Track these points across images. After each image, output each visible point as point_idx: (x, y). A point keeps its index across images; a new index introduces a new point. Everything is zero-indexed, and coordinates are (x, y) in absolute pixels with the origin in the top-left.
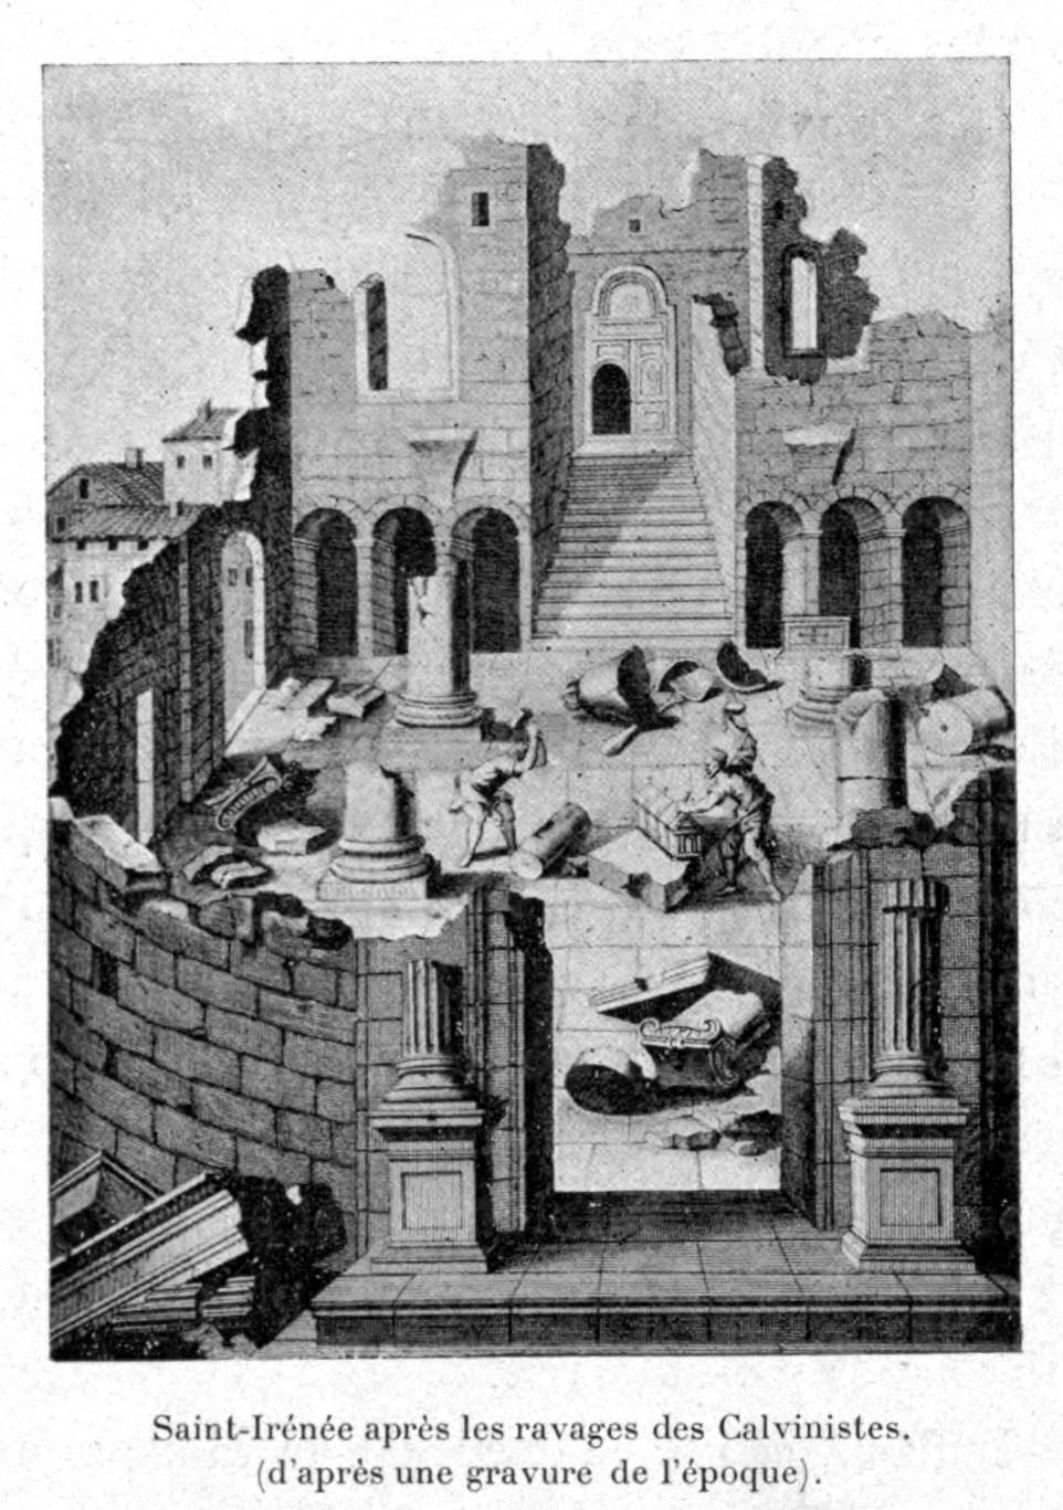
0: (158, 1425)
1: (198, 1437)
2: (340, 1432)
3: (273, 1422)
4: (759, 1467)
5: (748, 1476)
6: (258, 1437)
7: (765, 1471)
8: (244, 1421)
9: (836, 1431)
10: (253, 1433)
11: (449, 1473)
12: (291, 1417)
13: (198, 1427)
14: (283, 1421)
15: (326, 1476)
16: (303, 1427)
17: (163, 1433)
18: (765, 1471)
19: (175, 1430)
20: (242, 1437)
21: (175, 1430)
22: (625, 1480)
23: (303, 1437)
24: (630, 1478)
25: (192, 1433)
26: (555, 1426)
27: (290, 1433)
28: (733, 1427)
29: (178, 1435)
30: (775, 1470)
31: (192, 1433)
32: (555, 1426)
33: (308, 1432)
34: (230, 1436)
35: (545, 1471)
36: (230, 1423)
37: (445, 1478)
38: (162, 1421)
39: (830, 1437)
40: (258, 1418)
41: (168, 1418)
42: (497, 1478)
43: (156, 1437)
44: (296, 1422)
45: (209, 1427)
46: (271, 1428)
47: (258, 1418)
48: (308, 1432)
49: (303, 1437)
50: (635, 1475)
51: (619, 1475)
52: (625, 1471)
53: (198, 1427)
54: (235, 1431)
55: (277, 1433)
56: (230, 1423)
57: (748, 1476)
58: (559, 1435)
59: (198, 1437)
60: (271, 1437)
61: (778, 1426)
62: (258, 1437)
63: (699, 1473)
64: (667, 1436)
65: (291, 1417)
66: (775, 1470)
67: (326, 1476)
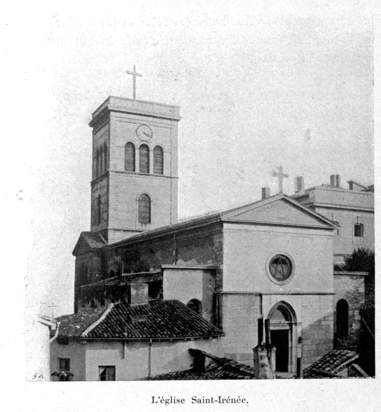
2: (242, 401)
6: (220, 402)
12: (229, 397)
16: (232, 400)
20: (215, 402)
23: (232, 402)
36: (212, 399)
38: (194, 398)
40: (220, 397)
46: (223, 400)
47: (220, 397)
49: (232, 402)
54: (213, 401)
56: (212, 399)
65: (229, 397)
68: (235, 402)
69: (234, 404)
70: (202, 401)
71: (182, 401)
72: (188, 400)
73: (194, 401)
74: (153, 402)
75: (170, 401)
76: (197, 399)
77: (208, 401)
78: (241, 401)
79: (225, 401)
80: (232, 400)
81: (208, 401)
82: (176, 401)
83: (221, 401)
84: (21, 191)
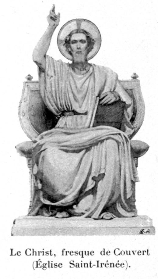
0: (71, 263)
1: (82, 267)
3: (102, 262)
4: (50, 268)
5: (81, 253)
6: (98, 266)
7: (85, 252)
8: (94, 263)
9: (53, 266)
11: (93, 252)
12: (107, 261)
13: (82, 264)
14: (105, 263)
16: (111, 264)
17: (72, 266)
18: (85, 252)
19: (75, 265)
20: (94, 266)
21: (75, 265)
22: (104, 254)
24: (105, 253)
25: (80, 266)
26: (133, 251)
27: (107, 266)
28: (117, 252)
29: (76, 266)
30: (88, 252)
31: (80, 266)
32: (133, 251)
33: (112, 265)
34: (90, 266)
37: (92, 254)
38: (72, 262)
39: (52, 267)
40: (98, 262)
43: (70, 267)
44: (109, 262)
45: (85, 264)
46: (101, 264)
47: (98, 262)
48: (112, 265)
49: (111, 267)
50: (107, 253)
51: (103, 253)
52: (104, 252)
53: (82, 264)
54: (92, 265)
55: (103, 266)
56: (90, 263)
57: (81, 253)
58: (134, 254)
59: (82, 267)
62: (98, 266)
63: (109, 264)
64: (104, 254)
65: (107, 261)
66: (88, 252)
69: (112, 268)
74: (12, 255)
76: (75, 263)
77: (86, 265)
78: (120, 265)
81: (86, 265)
83: (100, 265)
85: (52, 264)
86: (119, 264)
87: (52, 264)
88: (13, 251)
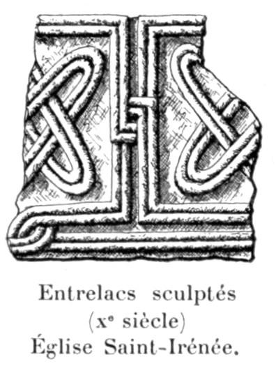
6: (172, 352)
10: (169, 349)
12: (217, 340)
15: (201, 295)
16: (201, 346)
19: (118, 348)
23: (201, 352)
27: (192, 350)
33: (204, 349)
35: (176, 292)
36: (152, 344)
40: (172, 340)
41: (114, 340)
42: (83, 296)
44: (197, 343)
45: (139, 346)
46: (180, 346)
47: (172, 340)
48: (204, 349)
54: (155, 348)
56: (152, 344)
60: (180, 352)
61: (100, 320)
62: (172, 352)
65: (217, 340)
67: (201, 295)
68: (207, 352)
70: (129, 350)
71: (86, 349)
72: (99, 347)
73: (110, 350)
75: (57, 349)
77: (60, 295)
79: (184, 350)
80: (201, 346)
81: (60, 295)
82: (72, 349)
83: (176, 349)
84: (236, 353)
85: (68, 346)
86: (224, 293)
87: (68, 346)
88: (175, 342)
